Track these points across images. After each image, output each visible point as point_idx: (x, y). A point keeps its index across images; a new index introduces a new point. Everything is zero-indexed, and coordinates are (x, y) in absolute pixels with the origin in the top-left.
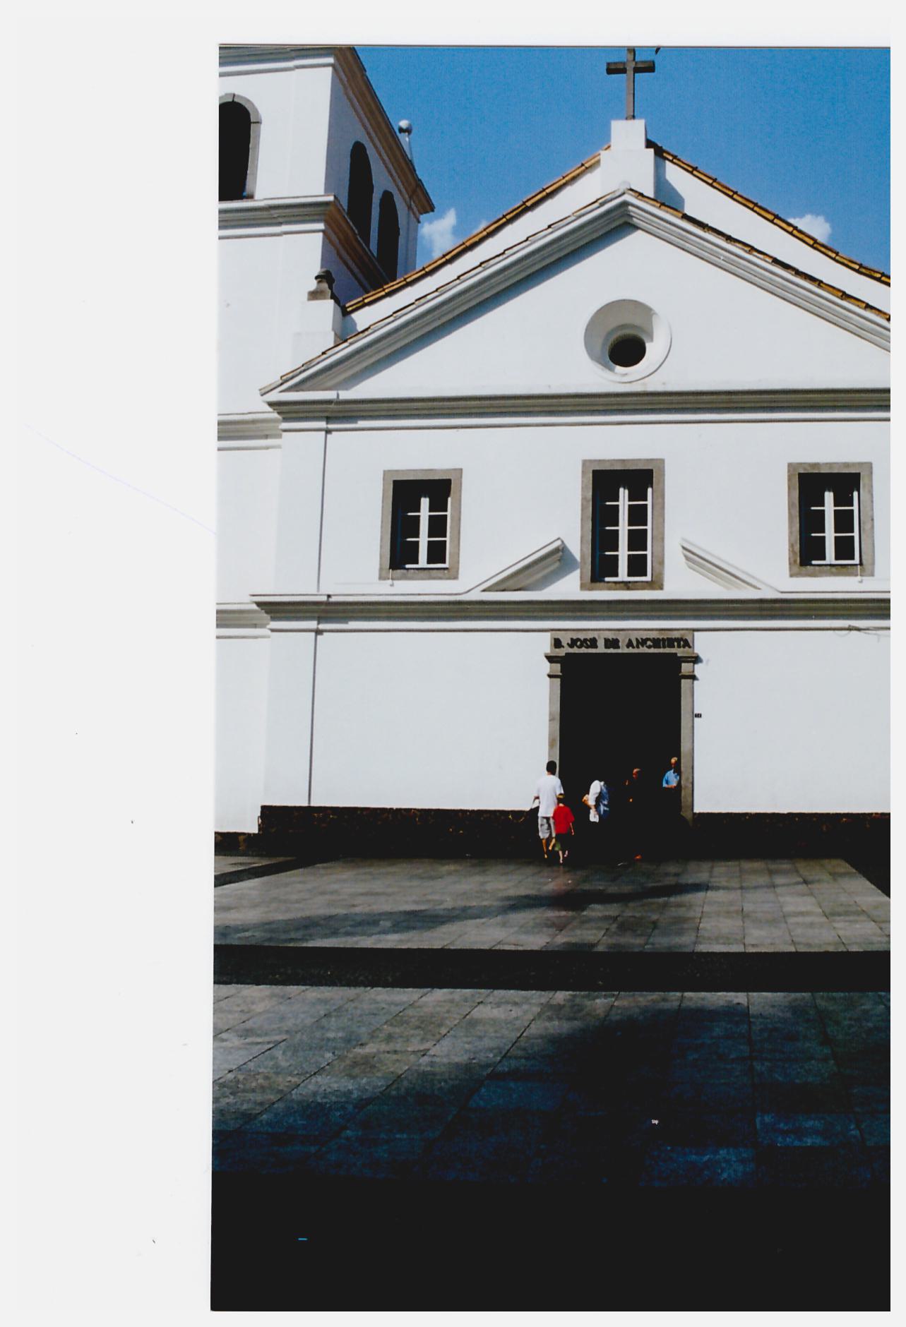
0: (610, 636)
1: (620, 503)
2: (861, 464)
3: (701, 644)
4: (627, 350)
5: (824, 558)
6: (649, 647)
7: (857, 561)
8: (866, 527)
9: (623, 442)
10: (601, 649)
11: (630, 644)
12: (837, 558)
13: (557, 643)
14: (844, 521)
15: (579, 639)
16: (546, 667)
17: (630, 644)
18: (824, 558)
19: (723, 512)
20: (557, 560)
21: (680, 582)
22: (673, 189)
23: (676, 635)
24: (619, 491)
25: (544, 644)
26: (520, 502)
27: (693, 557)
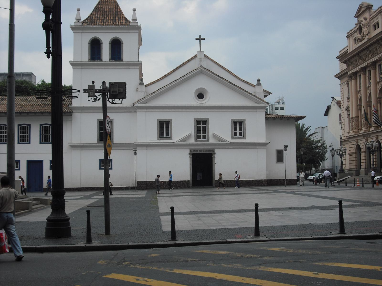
0: (200, 150)
1: (164, 127)
2: (98, 121)
3: (216, 151)
4: (201, 96)
5: (164, 136)
6: (207, 152)
7: (243, 136)
8: (244, 130)
9: (202, 115)
10: (198, 152)
11: (204, 151)
12: (166, 136)
13: (191, 151)
14: (240, 129)
15: (195, 150)
16: (189, 156)
17: (204, 151)
18: (164, 136)
19: (220, 128)
20: (189, 136)
21: (212, 141)
22: (9, 66)
23: (212, 150)
24: (202, 125)
25: (188, 151)
26: (183, 128)
27: (215, 136)
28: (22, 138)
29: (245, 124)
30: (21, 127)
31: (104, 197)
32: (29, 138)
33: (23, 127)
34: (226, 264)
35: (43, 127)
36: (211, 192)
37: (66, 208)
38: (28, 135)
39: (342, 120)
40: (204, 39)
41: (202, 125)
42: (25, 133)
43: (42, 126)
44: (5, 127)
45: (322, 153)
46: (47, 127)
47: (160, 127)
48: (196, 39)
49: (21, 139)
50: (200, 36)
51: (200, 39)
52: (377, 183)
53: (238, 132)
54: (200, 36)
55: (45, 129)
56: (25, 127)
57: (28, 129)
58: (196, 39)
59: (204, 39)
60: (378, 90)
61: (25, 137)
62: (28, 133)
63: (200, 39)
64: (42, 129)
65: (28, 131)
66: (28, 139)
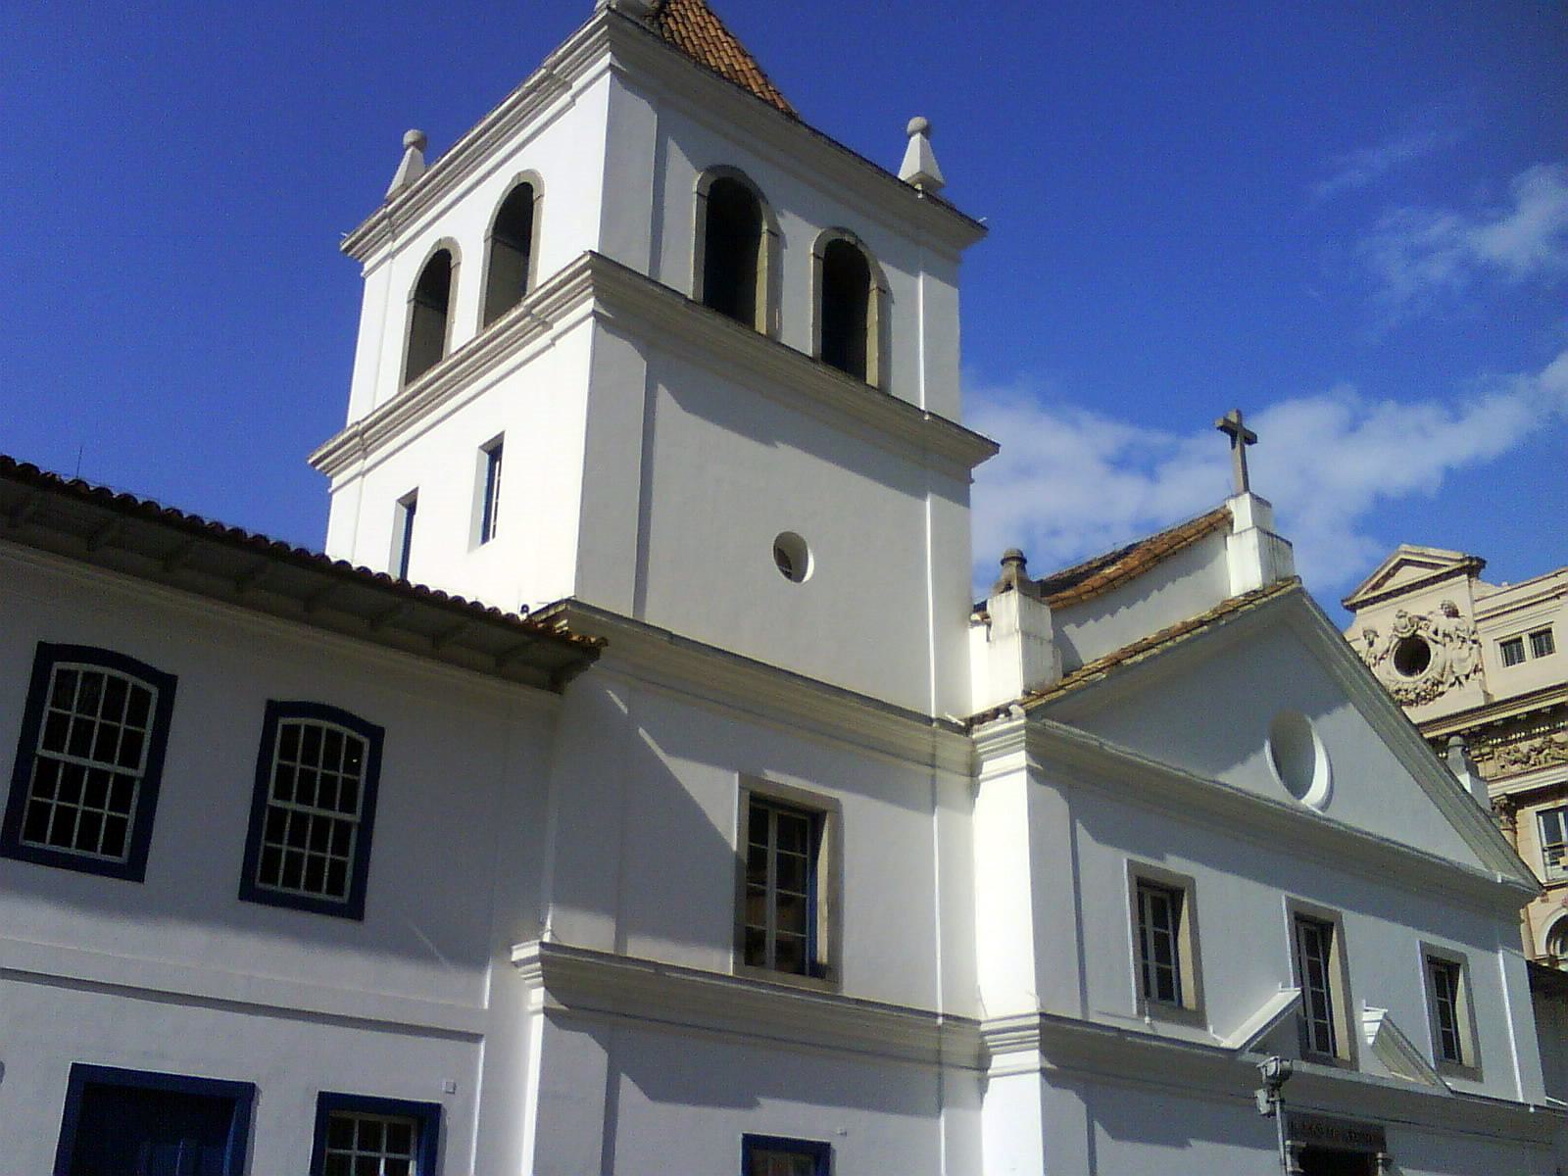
30: (291, 731)
31: (1251, 596)
32: (30, 797)
33: (92, 679)
34: (1336, 826)
36: (1440, 859)
37: (942, 284)
38: (124, 784)
39: (592, 319)
42: (103, 754)
43: (282, 721)
44: (324, 734)
45: (1551, 955)
46: (335, 737)
49: (272, 856)
52: (626, 494)
55: (310, 757)
56: (117, 685)
60: (530, 295)
61: (95, 799)
62: (130, 759)
64: (282, 756)
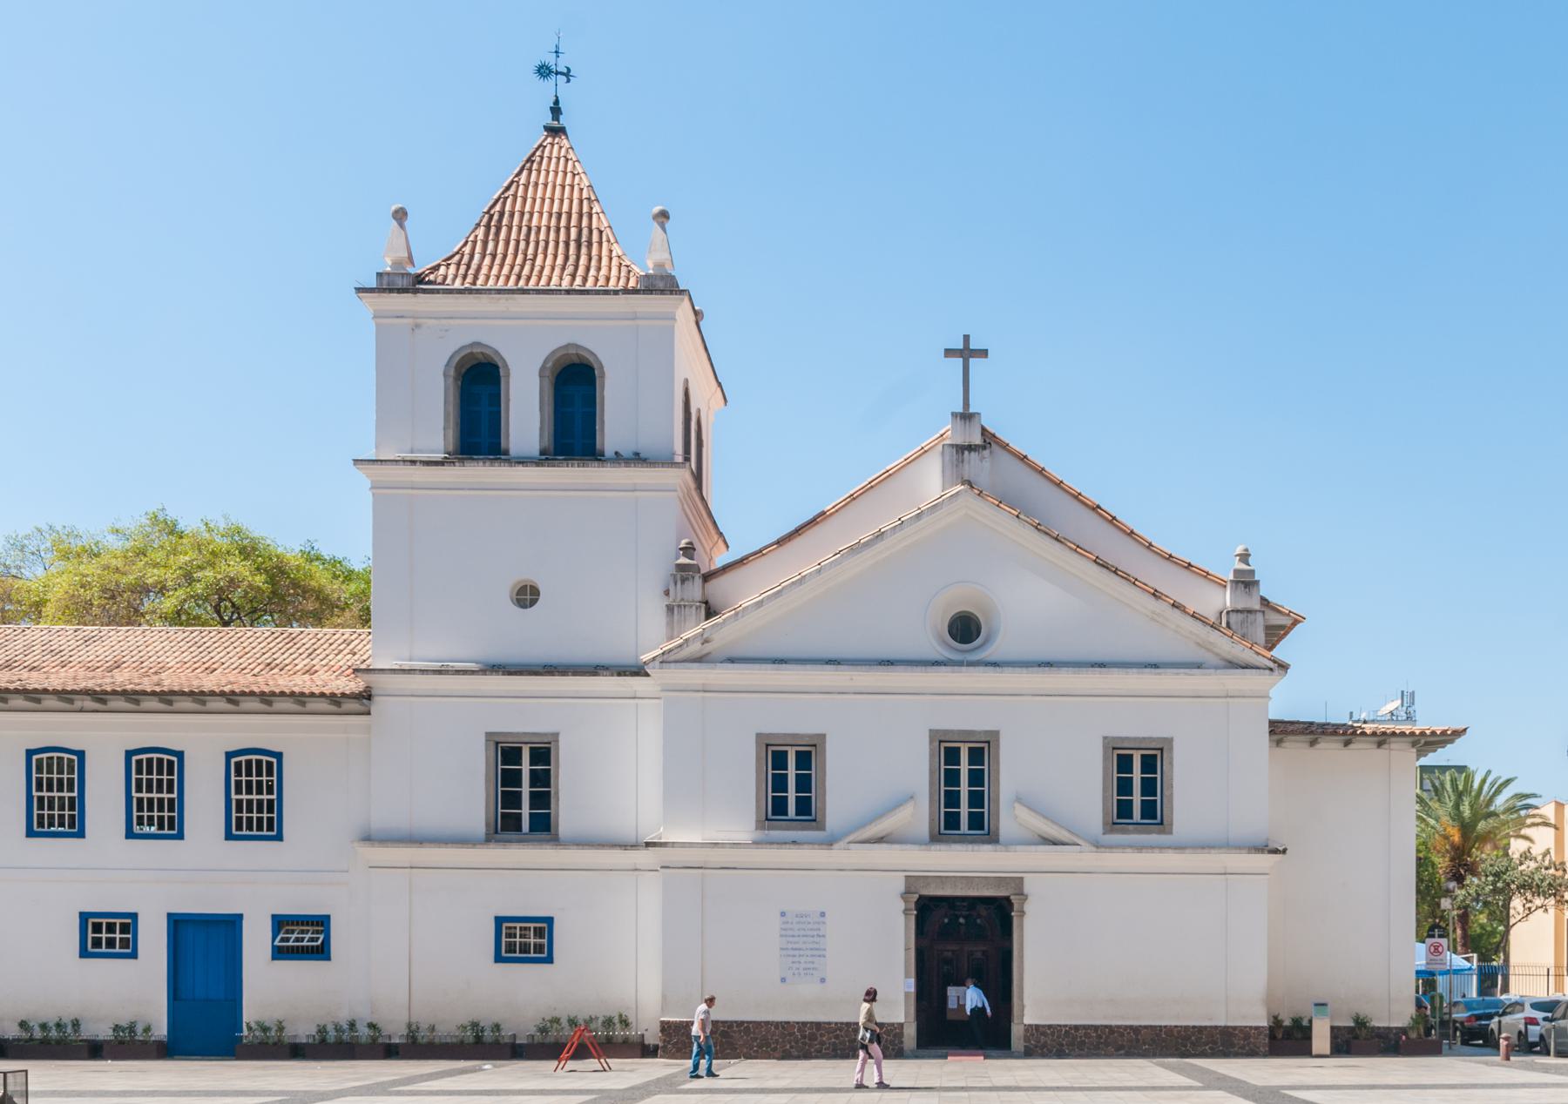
24: (964, 786)
28: (245, 815)
29: (1171, 763)
30: (39, 762)
35: (238, 765)
40: (983, 353)
41: (964, 786)
43: (134, 758)
46: (259, 762)
47: (1158, 798)
48: (949, 353)
49: (270, 810)
50: (966, 338)
51: (966, 353)
53: (792, 772)
54: (966, 338)
57: (170, 772)
58: (949, 353)
59: (983, 353)
63: (966, 353)
65: (170, 782)
66: (270, 820)
